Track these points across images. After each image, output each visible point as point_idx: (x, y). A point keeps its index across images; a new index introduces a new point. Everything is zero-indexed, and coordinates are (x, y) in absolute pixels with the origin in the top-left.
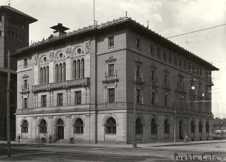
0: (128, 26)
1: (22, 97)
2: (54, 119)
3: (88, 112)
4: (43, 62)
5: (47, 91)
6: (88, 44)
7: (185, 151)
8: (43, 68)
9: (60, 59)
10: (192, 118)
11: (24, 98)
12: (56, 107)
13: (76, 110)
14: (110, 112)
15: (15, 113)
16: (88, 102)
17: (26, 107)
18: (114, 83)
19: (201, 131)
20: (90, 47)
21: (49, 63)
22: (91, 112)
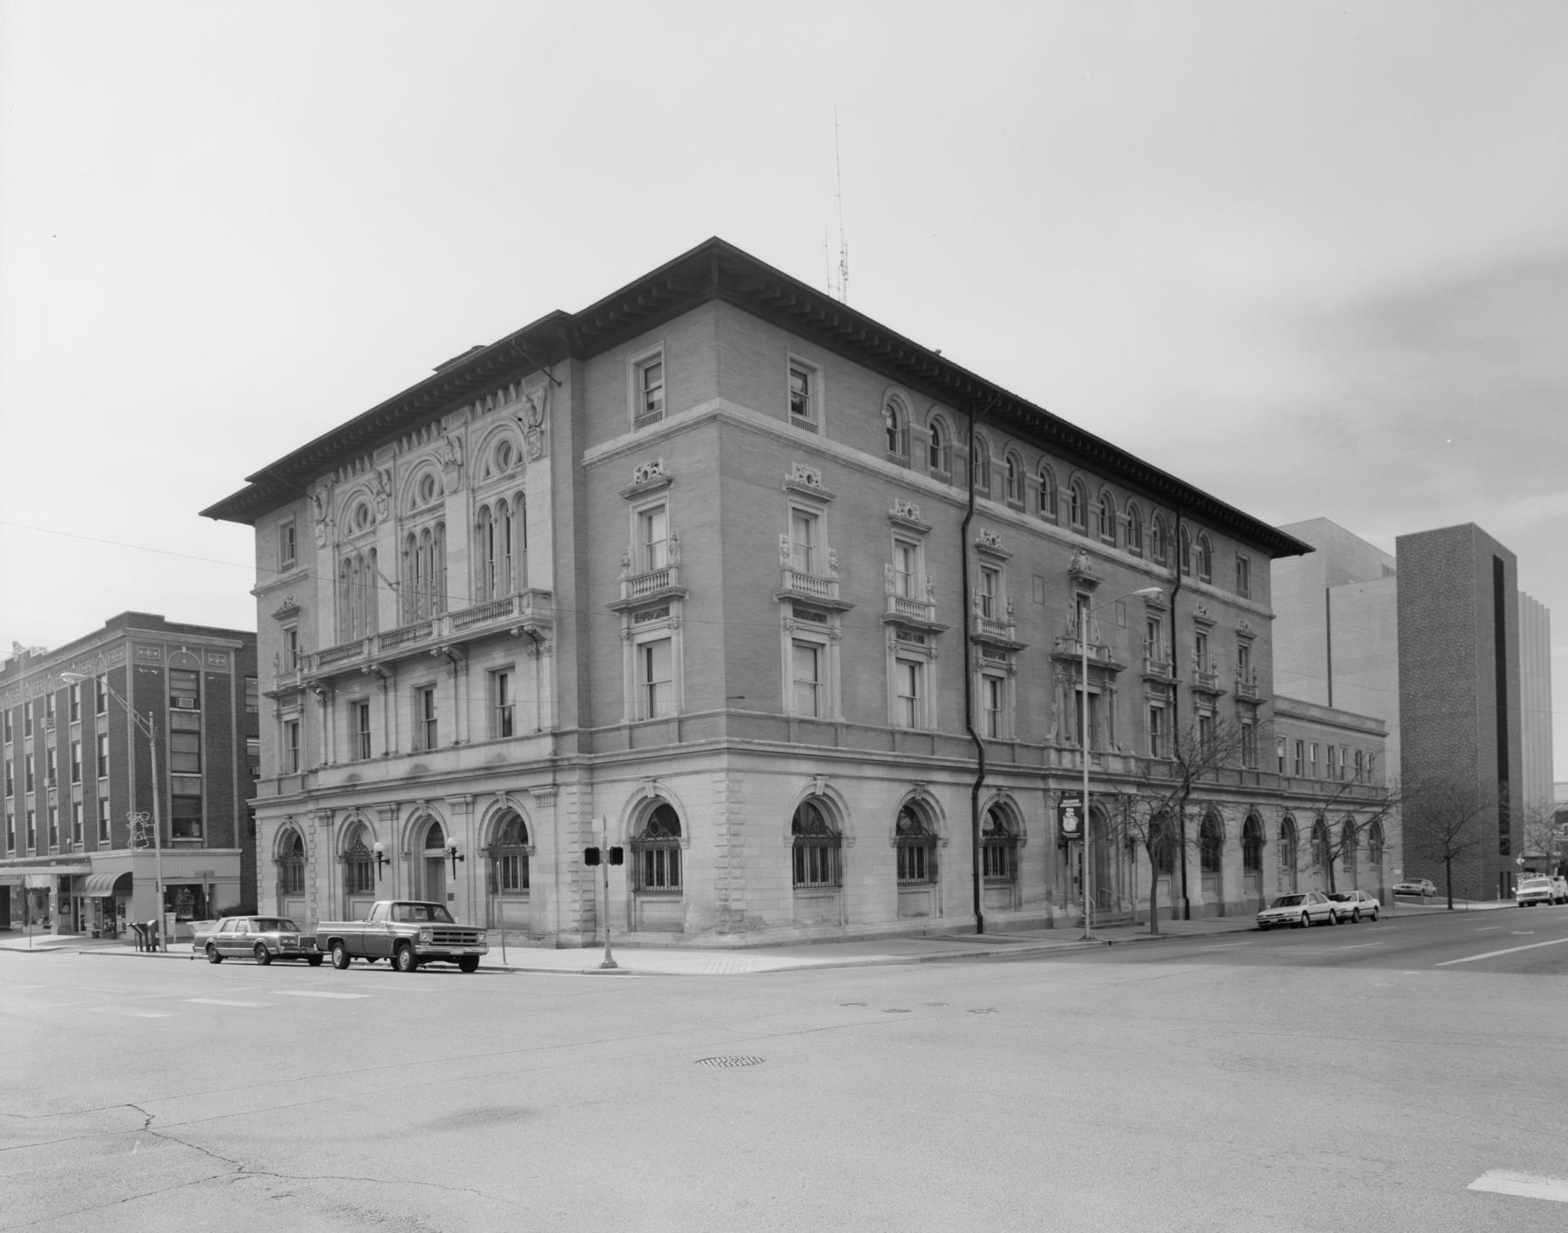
0: (715, 280)
1: (279, 716)
2: (337, 827)
3: (548, 778)
4: (493, 469)
5: (513, 637)
6: (539, 409)
7: (927, 965)
8: (509, 502)
9: (357, 533)
10: (994, 791)
11: (287, 718)
12: (484, 744)
13: (490, 772)
14: (653, 770)
15: (254, 795)
16: (547, 724)
17: (507, 727)
18: (666, 612)
19: (1252, 861)
20: (546, 426)
21: (442, 505)
22: (561, 778)
